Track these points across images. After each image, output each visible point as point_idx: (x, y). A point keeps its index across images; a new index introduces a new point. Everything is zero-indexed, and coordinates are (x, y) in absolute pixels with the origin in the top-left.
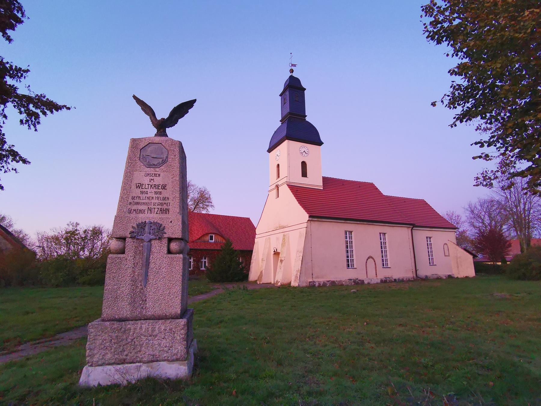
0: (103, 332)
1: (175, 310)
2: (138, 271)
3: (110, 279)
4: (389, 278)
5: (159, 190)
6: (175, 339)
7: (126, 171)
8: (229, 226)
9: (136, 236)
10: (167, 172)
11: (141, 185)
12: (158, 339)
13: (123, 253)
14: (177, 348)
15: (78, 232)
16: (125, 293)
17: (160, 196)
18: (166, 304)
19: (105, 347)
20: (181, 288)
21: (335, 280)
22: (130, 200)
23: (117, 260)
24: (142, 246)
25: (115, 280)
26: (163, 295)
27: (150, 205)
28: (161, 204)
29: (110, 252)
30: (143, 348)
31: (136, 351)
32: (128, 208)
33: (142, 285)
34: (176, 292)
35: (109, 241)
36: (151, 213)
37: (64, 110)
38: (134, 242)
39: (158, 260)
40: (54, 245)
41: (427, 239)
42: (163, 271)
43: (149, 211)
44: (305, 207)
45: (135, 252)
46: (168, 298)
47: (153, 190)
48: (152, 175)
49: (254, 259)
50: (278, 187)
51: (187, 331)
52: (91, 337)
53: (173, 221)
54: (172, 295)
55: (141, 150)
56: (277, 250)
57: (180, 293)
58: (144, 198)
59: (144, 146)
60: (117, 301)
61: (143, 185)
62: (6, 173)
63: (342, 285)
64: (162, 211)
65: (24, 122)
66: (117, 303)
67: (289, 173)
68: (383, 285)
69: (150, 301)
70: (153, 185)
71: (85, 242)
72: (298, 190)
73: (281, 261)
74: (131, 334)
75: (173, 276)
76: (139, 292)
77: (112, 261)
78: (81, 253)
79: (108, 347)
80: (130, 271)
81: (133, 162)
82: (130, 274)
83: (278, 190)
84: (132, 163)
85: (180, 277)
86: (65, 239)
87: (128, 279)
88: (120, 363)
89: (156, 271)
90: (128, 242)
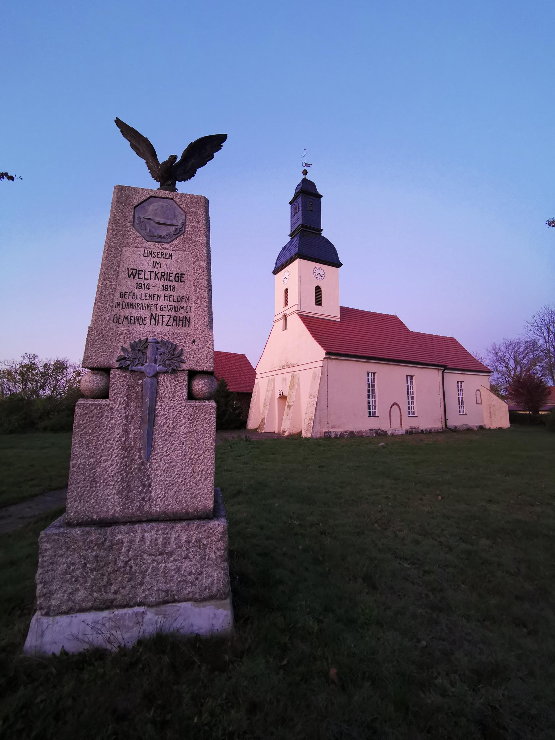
0: (68, 549)
1: (204, 502)
2: (135, 431)
3: (80, 445)
4: (415, 428)
5: (170, 283)
6: (207, 557)
8: (221, 363)
9: (129, 365)
10: (184, 251)
11: (138, 273)
12: (176, 560)
13: (105, 394)
14: (211, 576)
15: (36, 366)
16: (110, 471)
17: (173, 294)
18: (187, 492)
19: (73, 577)
20: (214, 462)
22: (117, 299)
23: (95, 410)
25: (91, 447)
26: (182, 475)
27: (155, 309)
28: (176, 309)
29: (81, 395)
30: (148, 578)
31: (133, 584)
32: (113, 313)
33: (143, 456)
34: (206, 470)
35: (75, 378)
36: (157, 323)
38: (125, 377)
39: (171, 411)
40: (6, 381)
41: (458, 383)
44: (404, 328)
45: (129, 394)
46: (190, 481)
47: (160, 283)
48: (158, 255)
49: (255, 401)
50: (286, 318)
51: (228, 543)
52: (45, 559)
53: (197, 341)
54: (198, 475)
55: (135, 208)
56: (283, 393)
57: (211, 471)
58: (144, 295)
59: (141, 200)
60: (96, 487)
61: (140, 272)
63: (362, 436)
64: (178, 322)
66: (95, 491)
67: (300, 300)
68: (409, 437)
69: (158, 486)
70: (160, 273)
71: (45, 379)
72: (311, 320)
73: (289, 406)
74: (123, 551)
75: (199, 440)
77: (84, 411)
78: (42, 392)
80: (118, 430)
81: (120, 228)
82: (120, 437)
83: (286, 320)
84: (119, 231)
85: (211, 443)
86: (19, 374)
87: (116, 444)
88: (104, 606)
89: (168, 431)
90: (115, 376)
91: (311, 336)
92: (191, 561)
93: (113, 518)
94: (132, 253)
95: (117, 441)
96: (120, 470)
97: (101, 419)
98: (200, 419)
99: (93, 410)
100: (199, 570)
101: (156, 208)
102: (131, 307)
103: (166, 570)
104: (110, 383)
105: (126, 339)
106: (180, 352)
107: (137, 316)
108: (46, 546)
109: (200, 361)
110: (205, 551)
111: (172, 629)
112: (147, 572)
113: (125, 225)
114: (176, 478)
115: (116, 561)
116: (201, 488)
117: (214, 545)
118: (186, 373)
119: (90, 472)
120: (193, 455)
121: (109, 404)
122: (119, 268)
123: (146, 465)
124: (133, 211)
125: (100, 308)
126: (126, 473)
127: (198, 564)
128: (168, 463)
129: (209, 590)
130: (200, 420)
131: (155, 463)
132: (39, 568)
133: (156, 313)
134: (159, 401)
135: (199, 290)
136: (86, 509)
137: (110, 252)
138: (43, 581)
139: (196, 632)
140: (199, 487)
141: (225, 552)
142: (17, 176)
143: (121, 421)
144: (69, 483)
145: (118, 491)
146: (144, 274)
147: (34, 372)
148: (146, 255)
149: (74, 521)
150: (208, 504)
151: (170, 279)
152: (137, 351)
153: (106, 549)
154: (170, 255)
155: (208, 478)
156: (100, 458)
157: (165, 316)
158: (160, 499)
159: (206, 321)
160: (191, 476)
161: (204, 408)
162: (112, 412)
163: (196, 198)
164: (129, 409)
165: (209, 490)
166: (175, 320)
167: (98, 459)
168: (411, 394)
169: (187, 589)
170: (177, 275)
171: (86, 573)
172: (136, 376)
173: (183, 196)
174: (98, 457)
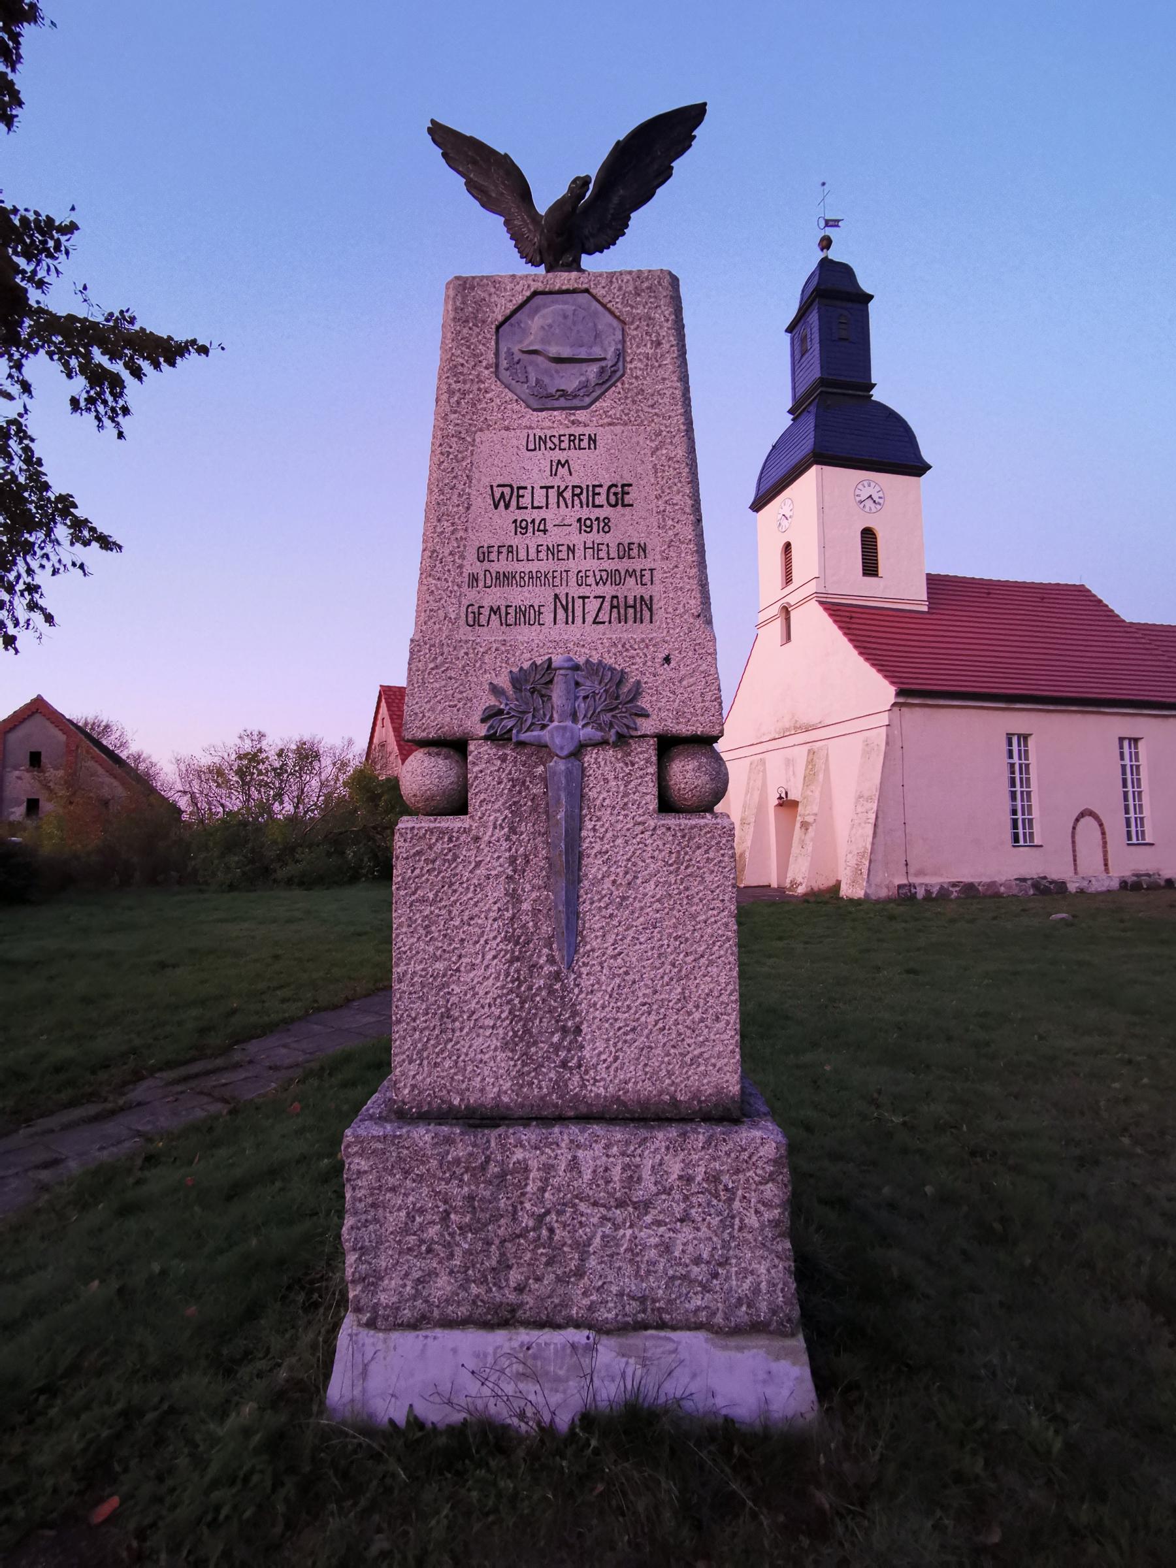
0: (406, 1173)
1: (715, 1077)
4: (1148, 875)
6: (737, 1221)
7: (442, 429)
9: (510, 730)
11: (515, 493)
12: (659, 1223)
13: (460, 807)
15: (264, 755)
16: (481, 993)
17: (607, 538)
18: (672, 1051)
21: (975, 880)
22: (472, 565)
23: (439, 845)
24: (544, 779)
25: (436, 935)
26: (655, 1007)
27: (564, 583)
28: (614, 577)
30: (592, 1262)
32: (465, 602)
33: (557, 958)
34: (716, 993)
37: (193, 357)
38: (503, 759)
39: (619, 841)
42: (645, 895)
43: (560, 612)
45: (515, 803)
46: (676, 1023)
48: (561, 441)
51: (790, 1188)
52: (360, 1194)
54: (697, 1007)
55: (498, 328)
57: (731, 998)
60: (453, 1031)
62: (57, 577)
63: (998, 895)
64: (622, 611)
65: (82, 404)
66: (451, 1040)
67: (823, 567)
68: (1131, 897)
69: (598, 1033)
71: (282, 781)
72: (854, 615)
73: (805, 825)
74: (529, 1189)
75: (693, 917)
76: (544, 993)
78: (276, 807)
79: (436, 1243)
80: (496, 892)
81: (467, 386)
82: (499, 909)
85: (726, 925)
86: (237, 773)
87: (492, 928)
88: (496, 1320)
89: (615, 893)
91: (855, 652)
92: (698, 1229)
93: (498, 1106)
94: (498, 446)
95: (495, 920)
96: (505, 991)
97: (453, 866)
98: (693, 862)
99: (434, 844)
100: (720, 1252)
101: (550, 321)
102: (506, 582)
103: (636, 1246)
104: (469, 776)
105: (498, 664)
106: (634, 689)
107: (521, 603)
108: (358, 1164)
109: (686, 710)
110: (730, 1205)
111: (662, 1400)
112: (590, 1245)
113: (478, 376)
114: (640, 1012)
115: (515, 1212)
116: (707, 1040)
117: (755, 1191)
118: (652, 742)
119: (438, 994)
120: (682, 956)
121: (470, 829)
122: (470, 487)
123: (567, 978)
124: (494, 337)
125: (432, 592)
126: (520, 997)
127: (715, 1239)
128: (619, 975)
129: (749, 1306)
130: (694, 866)
131: (587, 974)
132: (347, 1216)
133: (567, 594)
134: (589, 816)
135: (670, 522)
136: (435, 1082)
137: (447, 449)
138: (359, 1245)
139: (724, 1412)
140: (701, 1039)
141: (783, 1213)
142: (215, 344)
143: (500, 869)
144: (394, 1018)
145: (504, 1041)
146: (530, 496)
147: (261, 767)
148: (533, 447)
149: (411, 1108)
150: (727, 1081)
151: (597, 503)
152: (528, 694)
153: (490, 1183)
154: (593, 440)
155: (722, 1014)
156: (458, 961)
157: (589, 597)
158: (605, 1065)
159: (694, 604)
160: (678, 1010)
161: (702, 833)
162: (478, 847)
163: (647, 279)
164: (518, 839)
165: (726, 1045)
166: (615, 607)
167: (455, 963)
168: (1133, 787)
169: (691, 1298)
170: (613, 490)
171: (449, 1234)
172: (530, 756)
173: (614, 280)
174: (454, 959)
